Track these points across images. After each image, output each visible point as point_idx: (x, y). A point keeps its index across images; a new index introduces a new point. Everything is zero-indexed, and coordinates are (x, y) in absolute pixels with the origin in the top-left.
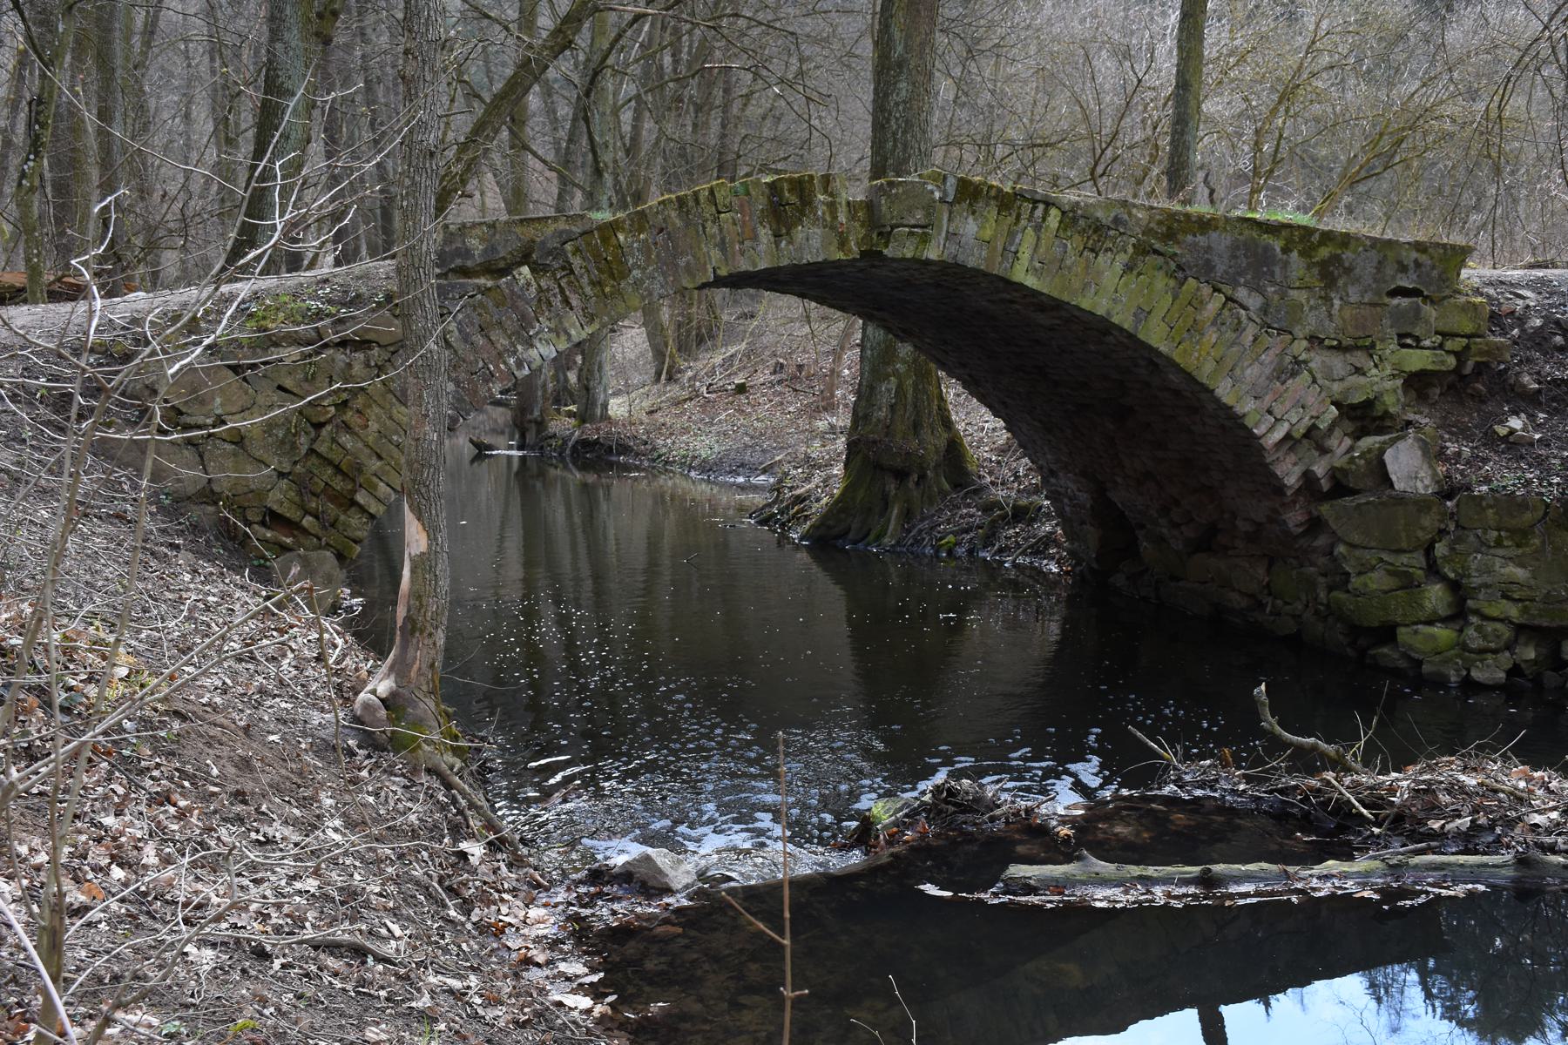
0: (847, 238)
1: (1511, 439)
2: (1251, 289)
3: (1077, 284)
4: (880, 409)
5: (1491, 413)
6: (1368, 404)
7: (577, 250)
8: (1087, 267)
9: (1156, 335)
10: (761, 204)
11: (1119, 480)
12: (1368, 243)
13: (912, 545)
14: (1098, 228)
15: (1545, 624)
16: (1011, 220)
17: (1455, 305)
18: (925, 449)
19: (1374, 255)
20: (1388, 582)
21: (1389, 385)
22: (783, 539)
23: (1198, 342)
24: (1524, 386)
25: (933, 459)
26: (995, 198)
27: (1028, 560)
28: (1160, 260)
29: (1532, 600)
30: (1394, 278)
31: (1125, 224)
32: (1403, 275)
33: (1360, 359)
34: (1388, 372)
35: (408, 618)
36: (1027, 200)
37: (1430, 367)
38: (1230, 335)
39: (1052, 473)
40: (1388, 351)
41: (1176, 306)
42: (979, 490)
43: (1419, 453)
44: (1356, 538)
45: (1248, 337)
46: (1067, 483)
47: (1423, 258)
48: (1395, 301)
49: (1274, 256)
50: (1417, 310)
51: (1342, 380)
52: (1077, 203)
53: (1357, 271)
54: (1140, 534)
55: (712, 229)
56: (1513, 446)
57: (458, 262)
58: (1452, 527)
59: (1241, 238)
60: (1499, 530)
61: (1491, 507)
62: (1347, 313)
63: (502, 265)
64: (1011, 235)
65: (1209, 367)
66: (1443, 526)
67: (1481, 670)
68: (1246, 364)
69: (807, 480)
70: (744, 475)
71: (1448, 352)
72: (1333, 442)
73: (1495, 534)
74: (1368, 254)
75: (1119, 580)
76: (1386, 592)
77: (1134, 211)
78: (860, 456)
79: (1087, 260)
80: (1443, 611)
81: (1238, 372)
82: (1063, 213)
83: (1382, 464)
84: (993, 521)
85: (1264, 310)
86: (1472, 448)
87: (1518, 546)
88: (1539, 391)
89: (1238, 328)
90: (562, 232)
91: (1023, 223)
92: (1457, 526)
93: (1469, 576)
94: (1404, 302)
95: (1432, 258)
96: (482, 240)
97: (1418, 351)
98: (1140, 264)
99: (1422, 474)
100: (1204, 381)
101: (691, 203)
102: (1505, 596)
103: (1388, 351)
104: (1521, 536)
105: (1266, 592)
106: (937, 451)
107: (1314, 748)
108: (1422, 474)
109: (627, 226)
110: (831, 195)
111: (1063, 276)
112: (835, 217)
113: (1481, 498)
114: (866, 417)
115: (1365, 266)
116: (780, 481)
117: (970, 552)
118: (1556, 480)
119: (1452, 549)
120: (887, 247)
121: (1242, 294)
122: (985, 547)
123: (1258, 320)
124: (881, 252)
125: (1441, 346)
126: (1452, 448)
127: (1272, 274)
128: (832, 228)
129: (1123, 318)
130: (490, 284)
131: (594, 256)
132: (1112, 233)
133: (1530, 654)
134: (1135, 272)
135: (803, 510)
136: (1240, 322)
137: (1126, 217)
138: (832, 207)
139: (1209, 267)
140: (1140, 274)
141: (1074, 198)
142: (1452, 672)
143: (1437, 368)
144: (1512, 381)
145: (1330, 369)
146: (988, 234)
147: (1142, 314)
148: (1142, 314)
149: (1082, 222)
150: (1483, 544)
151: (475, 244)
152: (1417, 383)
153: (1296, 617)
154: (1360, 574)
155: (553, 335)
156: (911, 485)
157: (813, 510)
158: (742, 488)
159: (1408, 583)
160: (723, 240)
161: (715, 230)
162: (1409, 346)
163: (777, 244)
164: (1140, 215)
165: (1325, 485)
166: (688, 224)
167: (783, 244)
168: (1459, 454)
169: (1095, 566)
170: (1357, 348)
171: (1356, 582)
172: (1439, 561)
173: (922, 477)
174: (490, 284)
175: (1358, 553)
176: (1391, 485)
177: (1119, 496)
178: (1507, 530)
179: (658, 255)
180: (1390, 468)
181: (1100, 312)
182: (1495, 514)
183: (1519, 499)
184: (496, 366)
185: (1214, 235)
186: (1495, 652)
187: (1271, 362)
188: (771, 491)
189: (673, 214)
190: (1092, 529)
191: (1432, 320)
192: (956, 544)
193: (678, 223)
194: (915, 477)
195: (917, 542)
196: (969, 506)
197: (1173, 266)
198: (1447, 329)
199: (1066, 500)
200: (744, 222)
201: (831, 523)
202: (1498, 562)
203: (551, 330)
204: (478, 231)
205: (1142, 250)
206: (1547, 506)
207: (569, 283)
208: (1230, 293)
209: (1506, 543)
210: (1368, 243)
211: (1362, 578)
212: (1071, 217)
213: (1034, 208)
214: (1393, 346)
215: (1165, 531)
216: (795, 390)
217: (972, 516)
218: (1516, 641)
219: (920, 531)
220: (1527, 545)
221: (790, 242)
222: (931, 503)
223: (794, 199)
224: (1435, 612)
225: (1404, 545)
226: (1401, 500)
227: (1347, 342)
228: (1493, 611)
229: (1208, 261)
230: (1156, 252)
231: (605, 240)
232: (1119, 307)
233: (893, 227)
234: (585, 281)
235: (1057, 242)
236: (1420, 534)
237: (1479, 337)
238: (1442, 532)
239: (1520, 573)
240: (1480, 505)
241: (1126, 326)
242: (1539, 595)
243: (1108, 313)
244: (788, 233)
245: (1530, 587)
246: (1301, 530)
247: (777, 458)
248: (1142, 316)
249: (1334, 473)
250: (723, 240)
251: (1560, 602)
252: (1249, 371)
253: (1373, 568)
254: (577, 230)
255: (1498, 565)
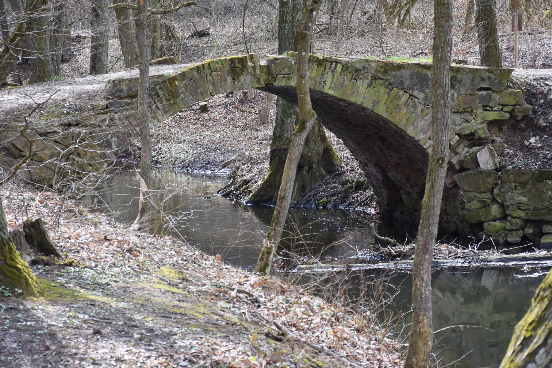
0: (260, 79)
1: (529, 147)
2: (420, 91)
3: (349, 92)
4: (287, 132)
5: (525, 136)
6: (472, 134)
7: (161, 88)
8: (353, 86)
9: (382, 111)
10: (227, 68)
11: (389, 167)
12: (467, 70)
13: (305, 203)
14: (357, 70)
15: (533, 219)
16: (322, 69)
17: (507, 93)
18: (311, 153)
19: (470, 75)
20: (479, 205)
21: (480, 126)
22: (238, 204)
23: (398, 112)
24: (540, 125)
25: (316, 158)
26: (316, 61)
27: (362, 208)
28: (382, 81)
29: (529, 210)
30: (479, 84)
31: (367, 68)
32: (483, 83)
33: (467, 116)
34: (480, 121)
35: (143, 208)
36: (329, 61)
37: (498, 118)
38: (411, 109)
39: (366, 165)
40: (479, 113)
41: (389, 99)
42: (341, 174)
43: (489, 153)
44: (466, 188)
45: (419, 110)
46: (372, 169)
47: (491, 75)
48: (481, 93)
49: (428, 78)
50: (490, 96)
51: (460, 125)
52: (348, 62)
53: (464, 82)
54: (402, 191)
55: (210, 78)
56: (530, 149)
57: (118, 94)
58: (500, 182)
59: (415, 71)
60: (515, 183)
61: (511, 174)
62: (460, 99)
63: (133, 94)
64: (323, 75)
65: (404, 122)
66: (496, 182)
67: (511, 238)
68: (419, 120)
69: (250, 171)
70: (210, 169)
71: (505, 112)
72: (459, 150)
73: (514, 184)
74: (468, 75)
75: (397, 214)
76: (478, 209)
77: (371, 63)
78: (277, 157)
79: (353, 83)
80: (498, 216)
81: (415, 123)
82: (343, 66)
83: (476, 158)
84: (346, 190)
85: (426, 98)
86: (514, 151)
87: (523, 189)
88: (546, 126)
89: (415, 106)
90: (155, 82)
91: (327, 70)
92: (502, 182)
93: (506, 201)
94: (484, 93)
95: (495, 75)
96: (127, 86)
97: (492, 112)
98: (374, 84)
99: (490, 162)
100: (402, 128)
101: (202, 69)
102: (519, 209)
103: (479, 113)
104: (523, 185)
105: (444, 213)
106: (318, 154)
107: (387, 240)
108: (490, 162)
109: (178, 79)
110: (253, 63)
111: (344, 89)
112: (255, 72)
113: (508, 170)
114: (280, 137)
115: (467, 79)
116: (235, 172)
117: (335, 206)
118: (539, 163)
119: (500, 191)
120: (275, 82)
121: (416, 93)
122: (342, 203)
123: (423, 103)
124: (273, 84)
125: (502, 110)
126: (507, 150)
127: (428, 85)
128: (254, 76)
129: (368, 105)
130: (129, 101)
131: (167, 90)
132: (362, 72)
133: (531, 231)
134: (372, 87)
135: (248, 188)
136: (415, 104)
137: (368, 66)
138: (254, 68)
139: (402, 83)
140: (374, 87)
141: (347, 59)
142: (501, 239)
143: (501, 119)
144: (535, 122)
145: (455, 121)
146: (314, 75)
147: (376, 103)
148: (376, 103)
149: (350, 69)
150: (510, 189)
151: (124, 87)
152: (492, 124)
153: (455, 223)
154: (469, 202)
155: (152, 119)
156: (304, 172)
157: (254, 187)
158: (210, 178)
159: (485, 205)
160: (214, 82)
161: (211, 78)
162: (488, 110)
163: (234, 82)
164: (373, 65)
165: (457, 167)
166: (201, 77)
167: (236, 83)
168: (508, 153)
169: (386, 208)
170: (465, 112)
171: (467, 206)
172: (495, 196)
173: (310, 168)
174: (129, 101)
175: (467, 194)
176: (479, 165)
177: (391, 174)
178: (518, 183)
179: (190, 89)
180: (479, 160)
181: (359, 103)
182: (514, 176)
183: (522, 171)
184: (132, 131)
185: (403, 71)
186: (516, 230)
187: (429, 119)
188: (229, 178)
189: (195, 73)
190: (384, 190)
191: (497, 100)
192: (327, 202)
193: (197, 76)
194: (307, 168)
195: (308, 202)
196: (335, 182)
197: (387, 83)
198: (503, 103)
199: (372, 177)
200: (221, 75)
201: (263, 193)
202: (516, 195)
203: (152, 118)
204: (125, 83)
205: (375, 78)
206: (533, 173)
207: (158, 100)
208: (411, 93)
209: (518, 188)
210: (467, 70)
211: (470, 204)
212: (346, 67)
213: (331, 64)
214: (481, 110)
215: (409, 189)
216: (242, 111)
217: (336, 188)
218: (525, 226)
219: (310, 196)
220: (526, 188)
221: (239, 82)
222: (316, 182)
223: (239, 66)
224: (495, 216)
225: (482, 190)
226: (481, 172)
227: (461, 110)
228: (515, 215)
229: (401, 82)
230: (380, 78)
231: (171, 84)
232: (366, 101)
233: (277, 75)
234: (164, 99)
235: (341, 77)
236: (488, 185)
237: (519, 105)
238: (496, 184)
239: (524, 199)
240: (508, 173)
241: (369, 108)
242: (531, 207)
243: (362, 103)
244: (238, 78)
245: (528, 205)
246: (451, 186)
247: (232, 158)
248: (376, 104)
249: (460, 162)
250: (214, 82)
251: (539, 210)
252: (420, 123)
253: (473, 200)
254: (160, 81)
255: (516, 196)
